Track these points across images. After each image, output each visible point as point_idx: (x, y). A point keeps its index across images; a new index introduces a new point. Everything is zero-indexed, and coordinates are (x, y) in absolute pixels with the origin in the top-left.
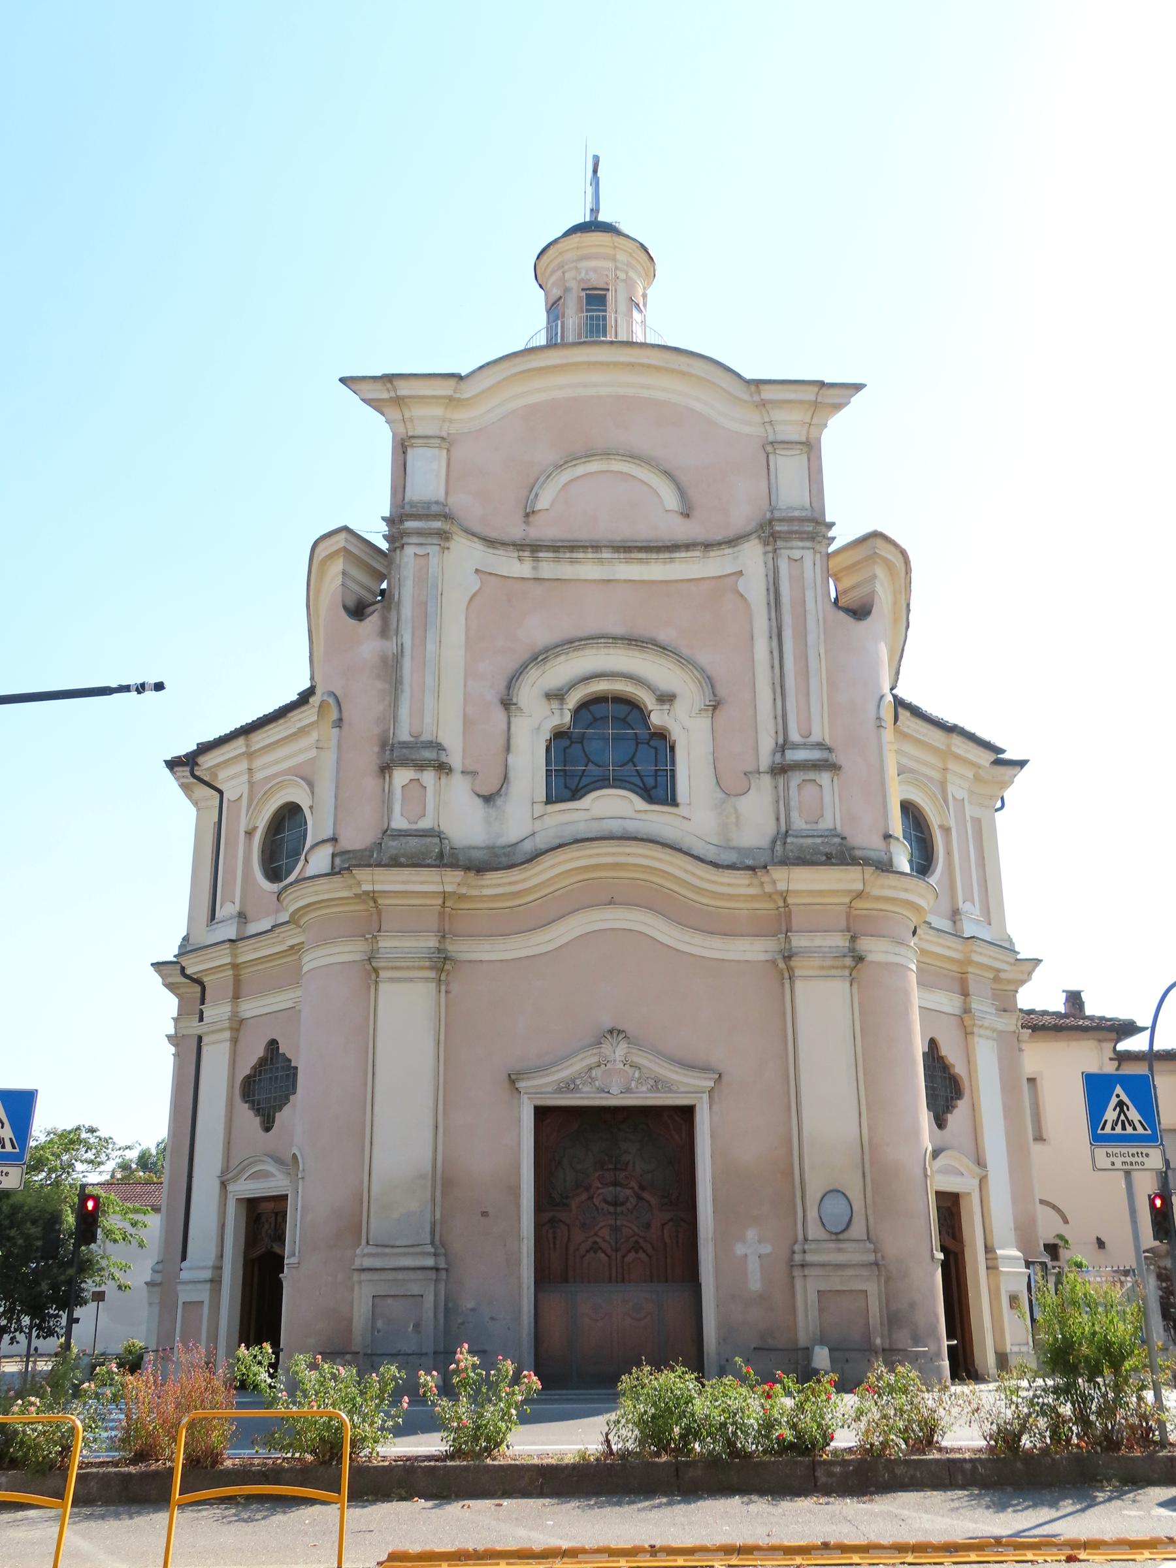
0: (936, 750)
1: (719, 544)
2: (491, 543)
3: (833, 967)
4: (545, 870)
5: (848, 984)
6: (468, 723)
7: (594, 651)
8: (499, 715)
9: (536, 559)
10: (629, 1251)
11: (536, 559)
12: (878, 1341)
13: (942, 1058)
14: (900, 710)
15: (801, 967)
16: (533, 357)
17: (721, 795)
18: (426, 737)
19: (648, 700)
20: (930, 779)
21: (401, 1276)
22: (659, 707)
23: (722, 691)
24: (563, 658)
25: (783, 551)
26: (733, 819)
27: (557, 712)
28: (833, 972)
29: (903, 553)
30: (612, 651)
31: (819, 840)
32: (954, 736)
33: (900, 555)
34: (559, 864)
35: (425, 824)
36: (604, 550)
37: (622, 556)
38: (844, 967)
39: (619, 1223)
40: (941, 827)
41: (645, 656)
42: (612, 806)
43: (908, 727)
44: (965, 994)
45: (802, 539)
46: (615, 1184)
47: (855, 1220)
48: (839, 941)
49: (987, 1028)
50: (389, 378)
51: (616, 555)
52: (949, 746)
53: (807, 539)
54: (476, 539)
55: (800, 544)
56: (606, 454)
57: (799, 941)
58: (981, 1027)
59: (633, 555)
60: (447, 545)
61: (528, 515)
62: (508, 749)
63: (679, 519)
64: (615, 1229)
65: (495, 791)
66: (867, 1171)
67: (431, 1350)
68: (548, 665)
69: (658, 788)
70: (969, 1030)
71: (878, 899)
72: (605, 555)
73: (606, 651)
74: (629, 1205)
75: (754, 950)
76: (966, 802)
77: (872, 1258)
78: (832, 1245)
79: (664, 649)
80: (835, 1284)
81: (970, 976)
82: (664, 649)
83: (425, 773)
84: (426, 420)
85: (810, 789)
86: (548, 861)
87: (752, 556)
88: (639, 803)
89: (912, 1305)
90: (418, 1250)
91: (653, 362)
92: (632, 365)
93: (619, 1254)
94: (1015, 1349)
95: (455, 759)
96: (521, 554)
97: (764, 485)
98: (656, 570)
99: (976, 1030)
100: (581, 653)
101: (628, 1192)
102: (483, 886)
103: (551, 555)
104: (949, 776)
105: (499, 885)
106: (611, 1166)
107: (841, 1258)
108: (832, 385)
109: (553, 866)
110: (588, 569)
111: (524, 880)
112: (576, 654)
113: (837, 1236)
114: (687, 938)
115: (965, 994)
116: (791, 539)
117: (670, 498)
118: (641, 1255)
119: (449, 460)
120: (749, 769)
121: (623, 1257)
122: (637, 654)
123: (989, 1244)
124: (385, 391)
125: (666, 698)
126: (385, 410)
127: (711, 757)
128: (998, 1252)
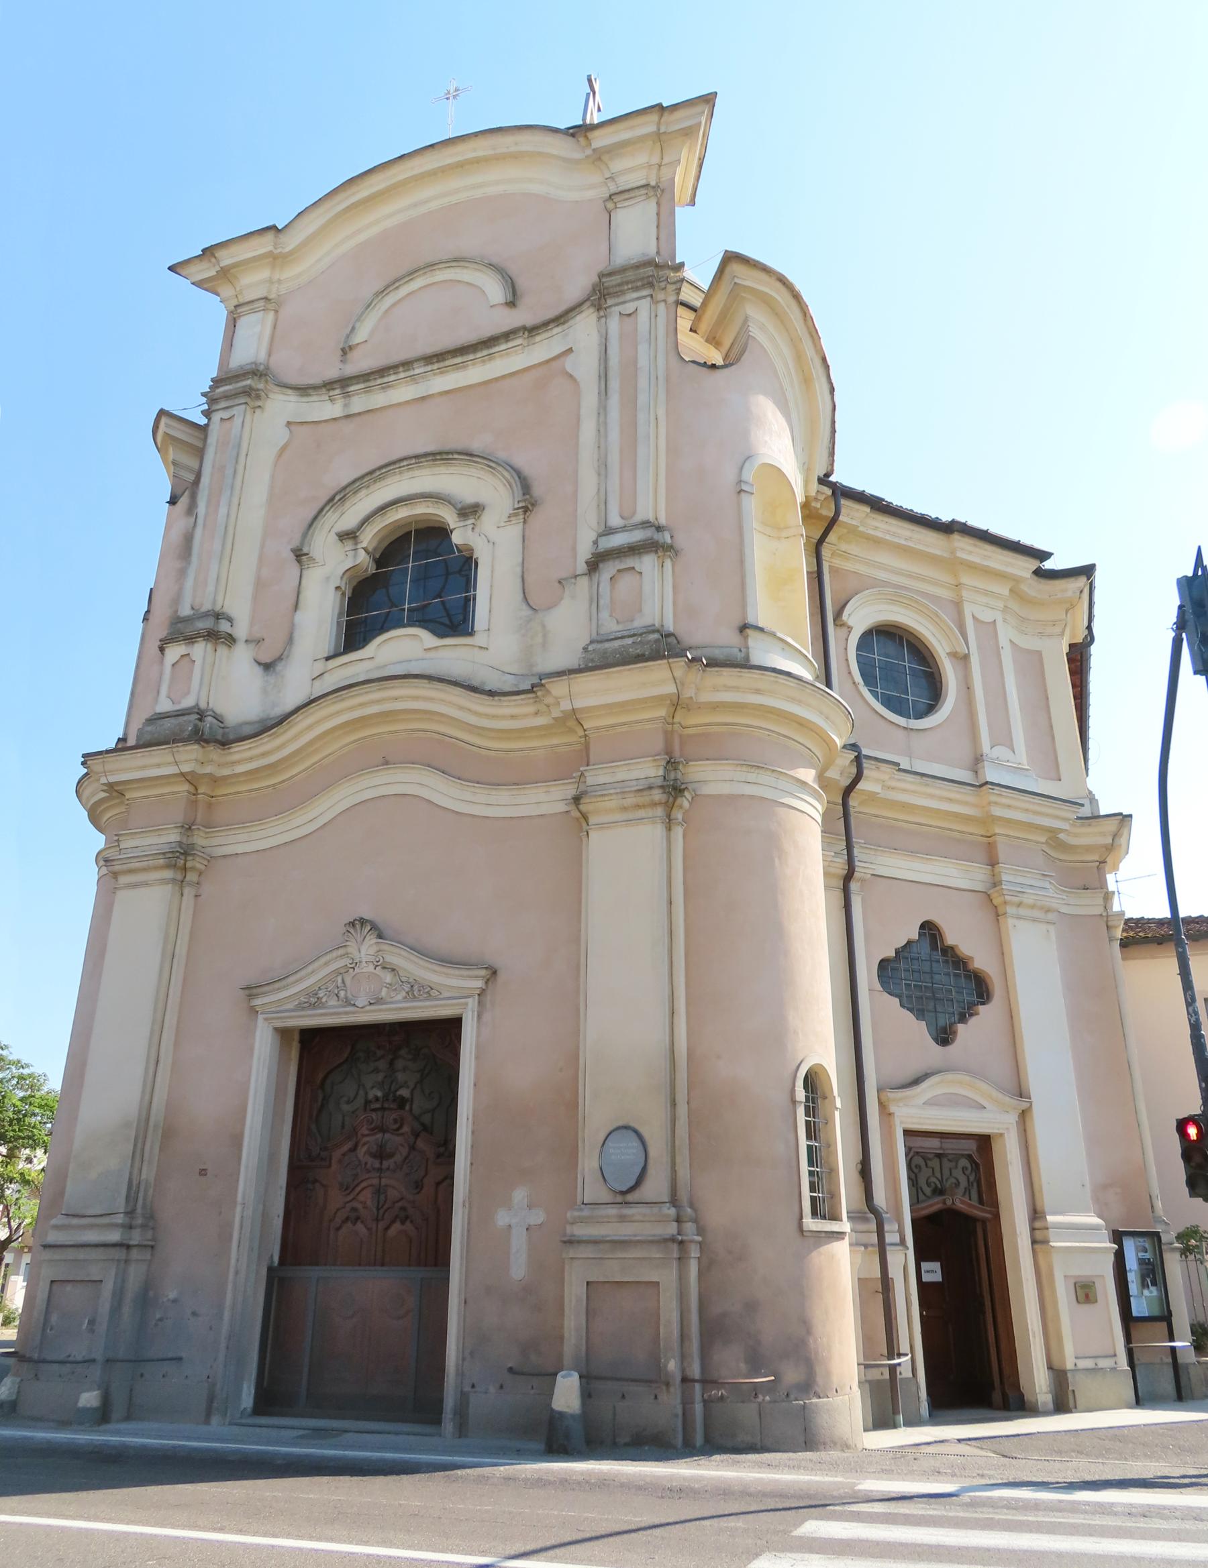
0: (933, 560)
1: (546, 325)
2: (303, 390)
3: (638, 806)
4: (301, 733)
5: (659, 830)
6: (260, 585)
7: (397, 478)
8: (294, 569)
9: (347, 395)
10: (393, 1222)
11: (347, 395)
12: (672, 1365)
13: (952, 948)
14: (843, 502)
15: (600, 809)
16: (354, 189)
17: (526, 612)
18: (207, 607)
19: (449, 517)
20: (934, 599)
21: (82, 1254)
22: (462, 524)
23: (537, 490)
24: (363, 492)
25: (613, 309)
26: (539, 639)
27: (351, 554)
28: (641, 813)
29: (782, 280)
30: (417, 473)
31: (629, 641)
32: (956, 537)
33: (779, 285)
34: (318, 722)
35: (188, 702)
36: (416, 365)
37: (435, 366)
38: (654, 804)
39: (384, 1182)
40: (953, 655)
41: (452, 470)
42: (403, 647)
43: (876, 528)
44: (993, 862)
45: (636, 289)
46: (383, 1129)
47: (651, 1171)
48: (651, 770)
49: (1033, 907)
50: (208, 252)
51: (429, 368)
52: (953, 552)
53: (643, 287)
54: (290, 392)
55: (635, 295)
56: (431, 266)
57: (595, 777)
58: (1019, 905)
59: (447, 363)
60: (259, 403)
61: (345, 351)
62: (296, 607)
63: (506, 311)
64: (379, 1191)
65: (278, 654)
66: (681, 1097)
67: (99, 1355)
68: (348, 504)
69: (454, 621)
70: (1000, 911)
71: (716, 707)
72: (417, 371)
73: (410, 474)
74: (398, 1158)
75: (548, 800)
76: (999, 624)
77: (672, 1229)
78: (613, 1211)
79: (471, 455)
80: (613, 1271)
81: (998, 838)
82: (471, 455)
83: (196, 645)
84: (253, 283)
85: (626, 581)
86: (302, 722)
87: (585, 327)
88: (426, 638)
89: (751, 1307)
90: (105, 1220)
91: (480, 153)
92: (460, 165)
93: (381, 1225)
94: (1083, 1364)
95: (241, 630)
96: (331, 393)
97: (604, 248)
98: (475, 373)
99: (1010, 910)
100: (383, 483)
101: (399, 1139)
102: (234, 763)
103: (362, 386)
104: (964, 593)
105: (251, 759)
106: (377, 1105)
107: (625, 1231)
108: (675, 107)
109: (310, 727)
110: (403, 392)
111: (279, 748)
112: (378, 485)
113: (626, 1194)
114: (468, 796)
115: (993, 862)
116: (623, 292)
117: (495, 291)
118: (359, 1226)
119: (276, 320)
120: (564, 575)
121: (387, 1228)
122: (443, 469)
123: (1038, 1208)
124: (210, 267)
125: (470, 511)
126: (219, 290)
127: (519, 569)
128: (1050, 1218)
